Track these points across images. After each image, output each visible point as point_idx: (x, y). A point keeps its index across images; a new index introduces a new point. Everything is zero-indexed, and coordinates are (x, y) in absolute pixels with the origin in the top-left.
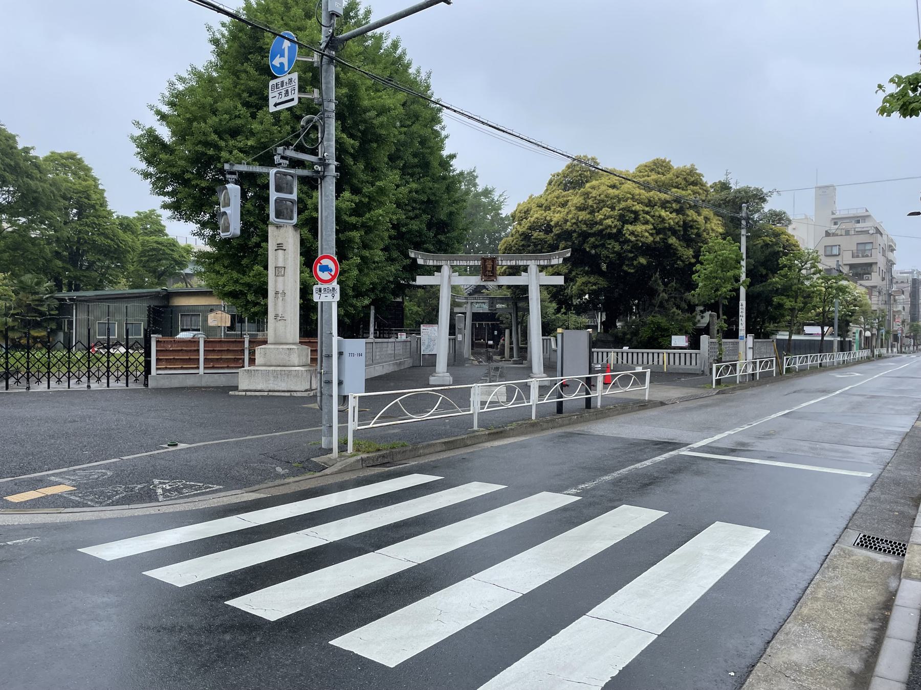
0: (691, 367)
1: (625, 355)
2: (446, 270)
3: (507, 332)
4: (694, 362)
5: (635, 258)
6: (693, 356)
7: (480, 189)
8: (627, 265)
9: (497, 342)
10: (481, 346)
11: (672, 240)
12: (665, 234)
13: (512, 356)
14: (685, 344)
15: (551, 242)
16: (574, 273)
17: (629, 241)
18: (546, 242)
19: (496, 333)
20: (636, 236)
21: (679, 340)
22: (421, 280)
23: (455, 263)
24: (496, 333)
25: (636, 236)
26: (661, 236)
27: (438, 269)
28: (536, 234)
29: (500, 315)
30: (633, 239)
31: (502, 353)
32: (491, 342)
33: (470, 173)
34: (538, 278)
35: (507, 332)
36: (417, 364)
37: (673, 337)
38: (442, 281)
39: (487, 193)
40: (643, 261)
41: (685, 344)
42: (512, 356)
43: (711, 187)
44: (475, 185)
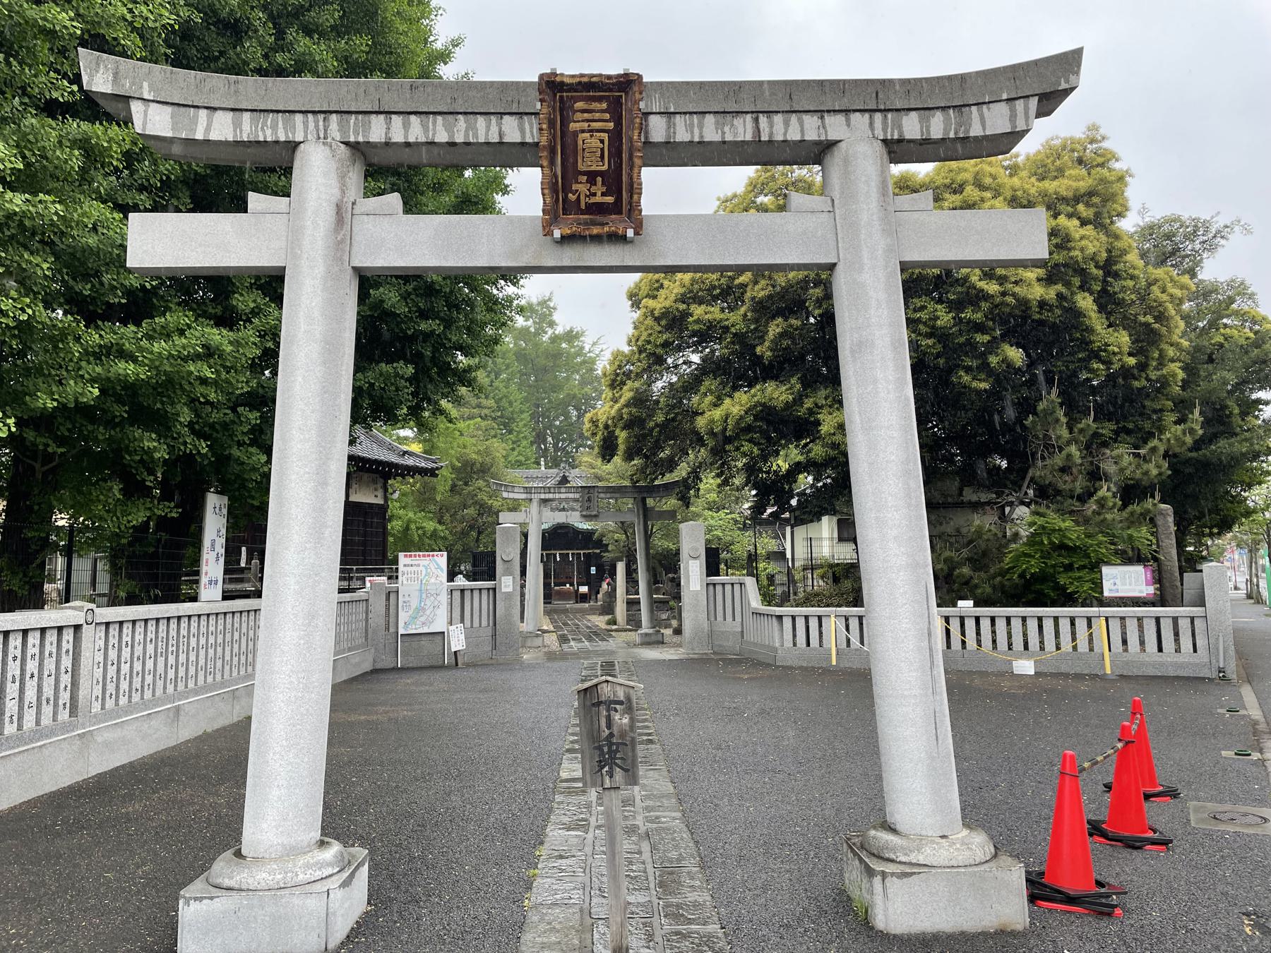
0: (1179, 659)
1: (970, 624)
2: (320, 173)
3: (621, 568)
4: (1186, 643)
5: (992, 346)
6: (1184, 625)
7: (559, 330)
8: (968, 370)
9: (595, 590)
10: (564, 596)
11: (1085, 302)
12: (1067, 284)
13: (634, 622)
14: (1148, 590)
15: (741, 327)
16: (808, 403)
17: (983, 296)
18: (726, 329)
19: (593, 570)
20: (1002, 280)
21: (1125, 580)
22: (162, 242)
23: (376, 131)
24: (593, 570)
25: (1002, 280)
26: (1059, 287)
27: (271, 170)
28: (698, 311)
29: (603, 535)
30: (993, 288)
31: (608, 609)
32: (584, 589)
33: (543, 303)
34: (891, 228)
35: (621, 568)
36: (387, 662)
37: (1106, 570)
38: (294, 238)
39: (571, 336)
40: (1015, 355)
41: (1148, 590)
42: (634, 622)
43: (1050, 254)
44: (552, 324)
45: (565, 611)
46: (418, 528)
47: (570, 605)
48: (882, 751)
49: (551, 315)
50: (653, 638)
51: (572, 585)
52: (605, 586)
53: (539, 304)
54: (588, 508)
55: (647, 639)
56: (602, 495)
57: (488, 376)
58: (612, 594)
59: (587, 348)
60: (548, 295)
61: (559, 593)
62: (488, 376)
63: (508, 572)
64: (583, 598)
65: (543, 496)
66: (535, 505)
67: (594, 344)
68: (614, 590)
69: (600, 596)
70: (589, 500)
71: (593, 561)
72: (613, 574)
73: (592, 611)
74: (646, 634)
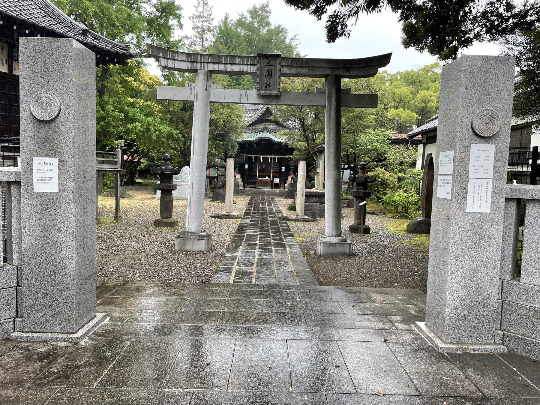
3: (302, 166)
9: (284, 181)
19: (283, 169)
24: (283, 169)
31: (291, 194)
32: (277, 180)
35: (302, 166)
44: (268, 24)
45: (264, 193)
46: (156, 130)
47: (268, 190)
48: (334, 200)
49: (267, 17)
50: (339, 249)
51: (269, 177)
52: (290, 179)
53: (261, 9)
54: (267, 86)
55: (331, 250)
56: (286, 70)
57: (228, 49)
58: (294, 185)
59: (287, 41)
60: (266, 3)
61: (261, 181)
62: (228, 49)
63: (48, 148)
64: (276, 186)
65: (211, 67)
66: (200, 79)
67: (292, 39)
68: (296, 182)
69: (286, 185)
70: (269, 74)
71: (283, 164)
72: (296, 171)
73: (280, 195)
74: (330, 244)
